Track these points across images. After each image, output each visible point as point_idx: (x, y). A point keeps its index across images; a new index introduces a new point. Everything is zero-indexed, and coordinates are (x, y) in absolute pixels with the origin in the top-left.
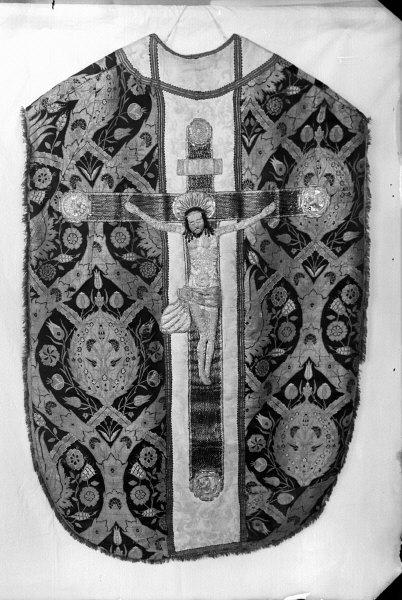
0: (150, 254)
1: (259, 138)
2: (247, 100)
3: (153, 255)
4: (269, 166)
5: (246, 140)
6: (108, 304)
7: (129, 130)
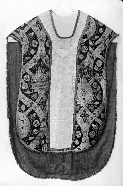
1: (88, 118)
2: (83, 106)
5: (84, 118)
6: (20, 109)
7: (30, 57)
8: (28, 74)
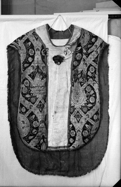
0: (34, 95)
1: (81, 119)
3: (35, 95)
4: (85, 126)
8: (27, 79)
